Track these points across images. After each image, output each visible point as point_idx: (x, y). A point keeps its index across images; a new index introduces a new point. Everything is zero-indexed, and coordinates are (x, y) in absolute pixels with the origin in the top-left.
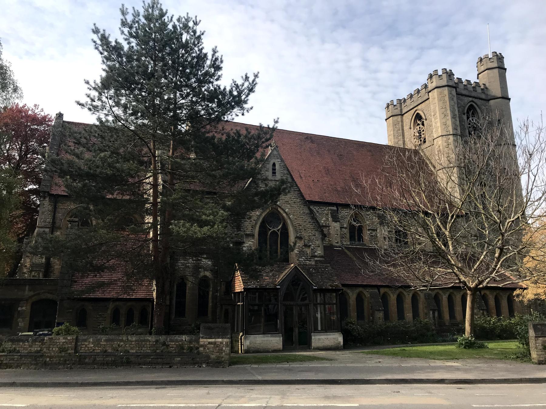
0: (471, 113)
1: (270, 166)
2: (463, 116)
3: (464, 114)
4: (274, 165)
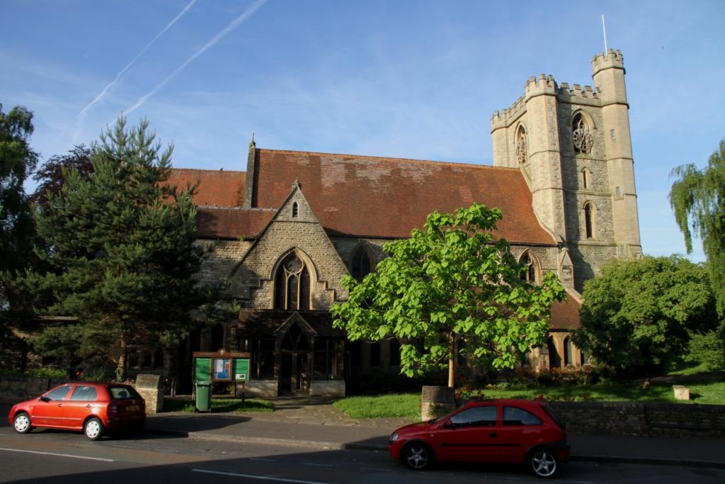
0: (579, 124)
1: (290, 207)
2: (568, 127)
3: (569, 125)
4: (295, 205)
